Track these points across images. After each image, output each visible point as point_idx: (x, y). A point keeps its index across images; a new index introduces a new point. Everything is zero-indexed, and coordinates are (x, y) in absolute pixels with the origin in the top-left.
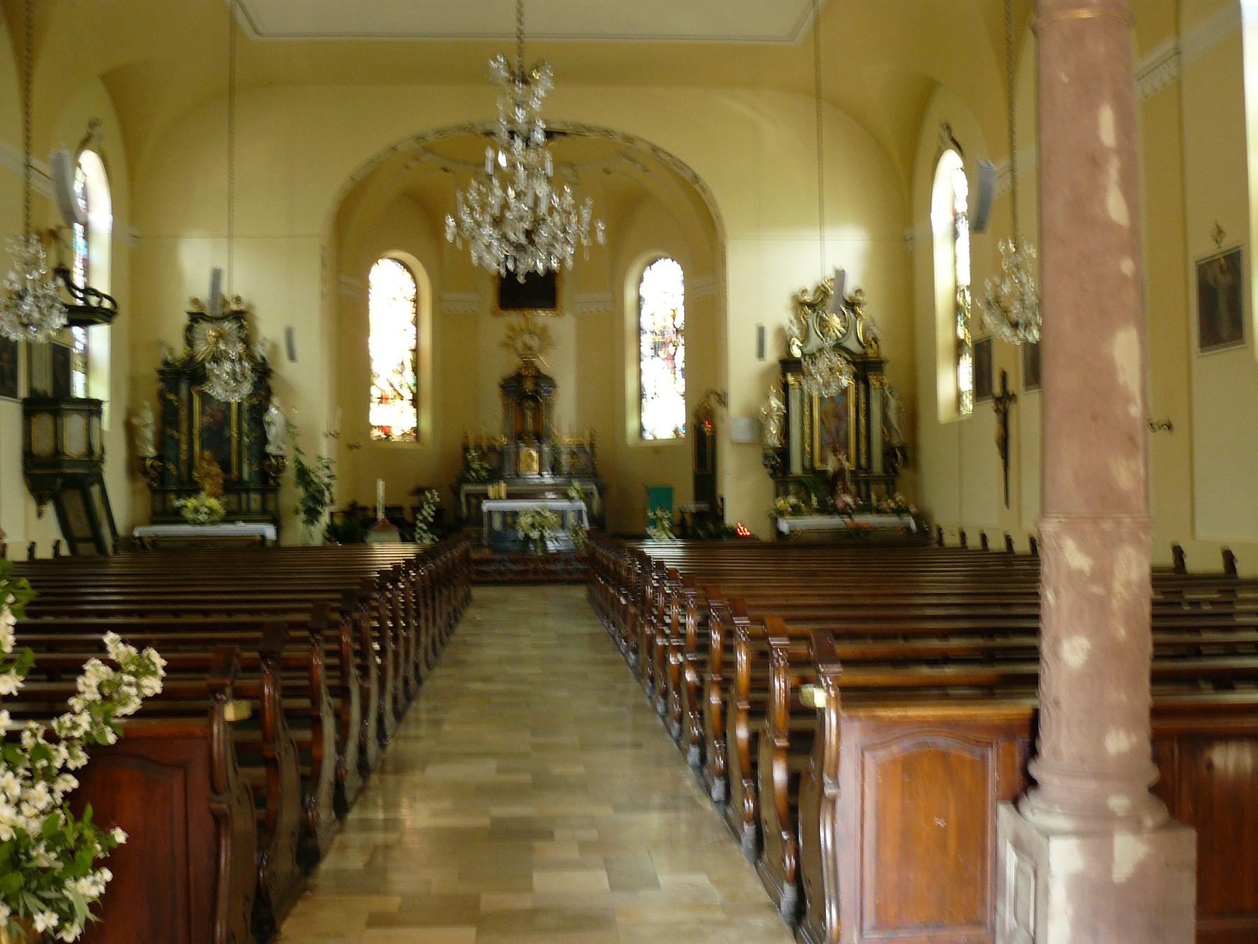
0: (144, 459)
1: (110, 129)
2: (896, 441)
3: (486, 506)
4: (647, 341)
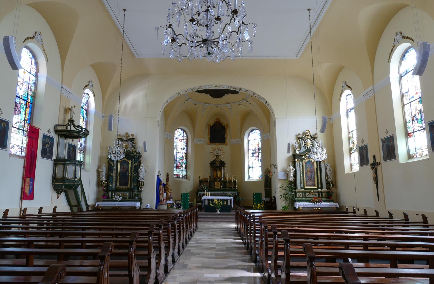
0: (102, 181)
1: (96, 83)
2: (329, 180)
3: (203, 198)
4: (250, 152)
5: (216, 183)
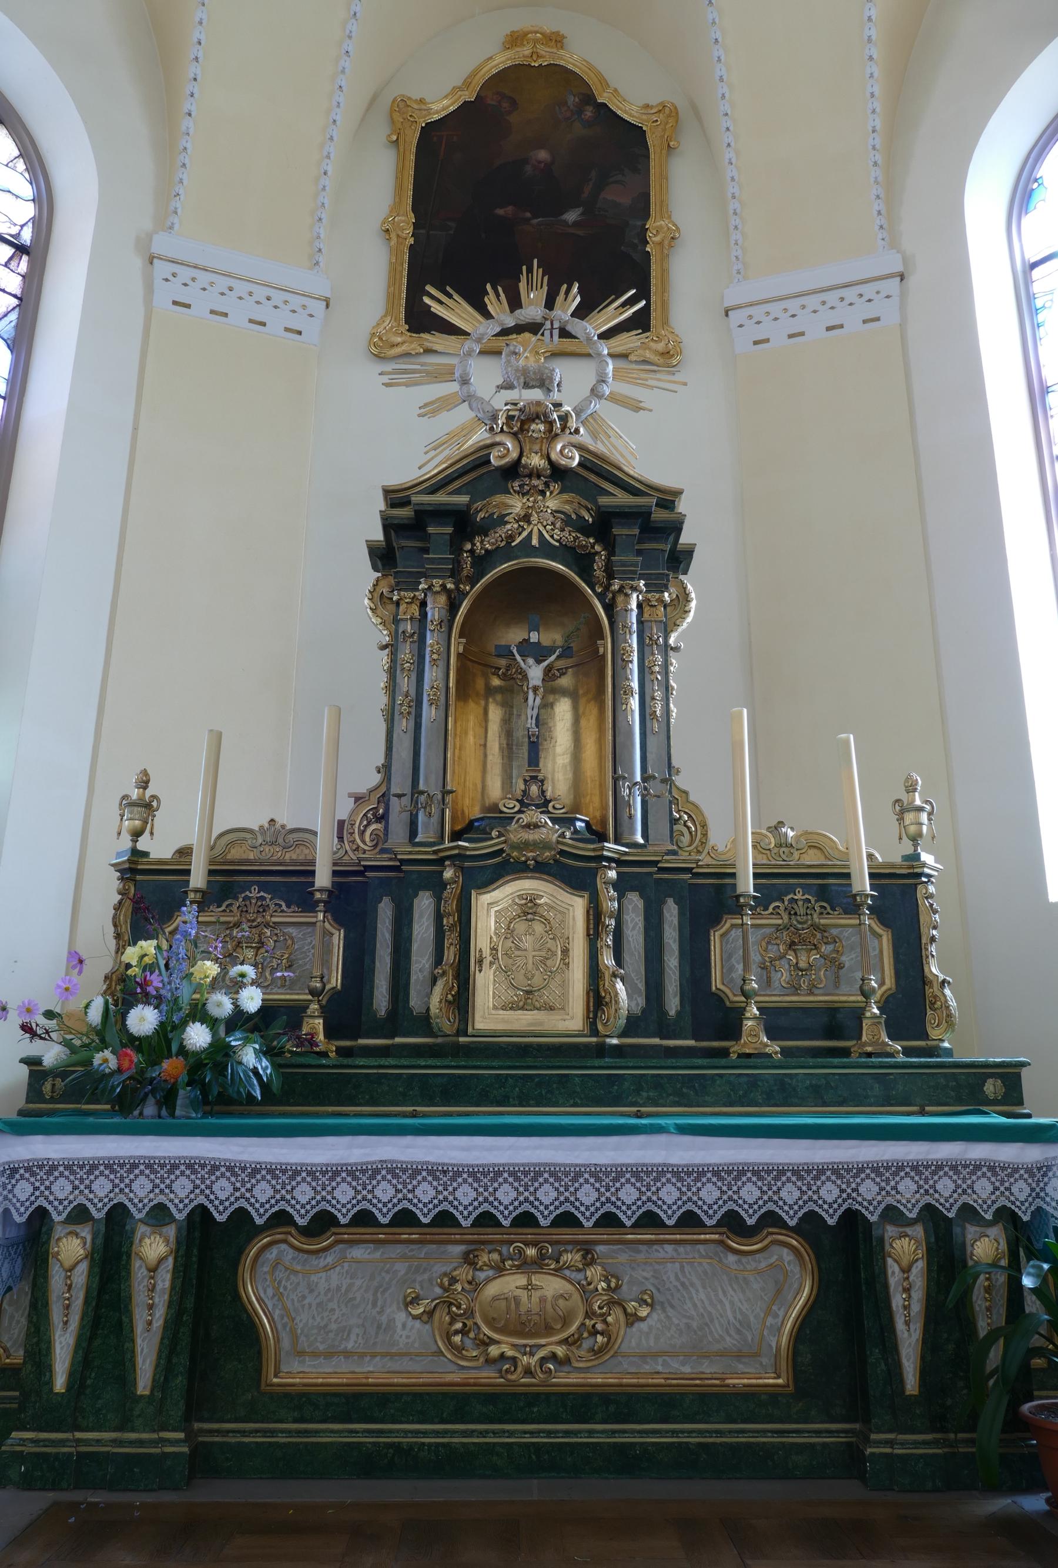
5: (492, 909)
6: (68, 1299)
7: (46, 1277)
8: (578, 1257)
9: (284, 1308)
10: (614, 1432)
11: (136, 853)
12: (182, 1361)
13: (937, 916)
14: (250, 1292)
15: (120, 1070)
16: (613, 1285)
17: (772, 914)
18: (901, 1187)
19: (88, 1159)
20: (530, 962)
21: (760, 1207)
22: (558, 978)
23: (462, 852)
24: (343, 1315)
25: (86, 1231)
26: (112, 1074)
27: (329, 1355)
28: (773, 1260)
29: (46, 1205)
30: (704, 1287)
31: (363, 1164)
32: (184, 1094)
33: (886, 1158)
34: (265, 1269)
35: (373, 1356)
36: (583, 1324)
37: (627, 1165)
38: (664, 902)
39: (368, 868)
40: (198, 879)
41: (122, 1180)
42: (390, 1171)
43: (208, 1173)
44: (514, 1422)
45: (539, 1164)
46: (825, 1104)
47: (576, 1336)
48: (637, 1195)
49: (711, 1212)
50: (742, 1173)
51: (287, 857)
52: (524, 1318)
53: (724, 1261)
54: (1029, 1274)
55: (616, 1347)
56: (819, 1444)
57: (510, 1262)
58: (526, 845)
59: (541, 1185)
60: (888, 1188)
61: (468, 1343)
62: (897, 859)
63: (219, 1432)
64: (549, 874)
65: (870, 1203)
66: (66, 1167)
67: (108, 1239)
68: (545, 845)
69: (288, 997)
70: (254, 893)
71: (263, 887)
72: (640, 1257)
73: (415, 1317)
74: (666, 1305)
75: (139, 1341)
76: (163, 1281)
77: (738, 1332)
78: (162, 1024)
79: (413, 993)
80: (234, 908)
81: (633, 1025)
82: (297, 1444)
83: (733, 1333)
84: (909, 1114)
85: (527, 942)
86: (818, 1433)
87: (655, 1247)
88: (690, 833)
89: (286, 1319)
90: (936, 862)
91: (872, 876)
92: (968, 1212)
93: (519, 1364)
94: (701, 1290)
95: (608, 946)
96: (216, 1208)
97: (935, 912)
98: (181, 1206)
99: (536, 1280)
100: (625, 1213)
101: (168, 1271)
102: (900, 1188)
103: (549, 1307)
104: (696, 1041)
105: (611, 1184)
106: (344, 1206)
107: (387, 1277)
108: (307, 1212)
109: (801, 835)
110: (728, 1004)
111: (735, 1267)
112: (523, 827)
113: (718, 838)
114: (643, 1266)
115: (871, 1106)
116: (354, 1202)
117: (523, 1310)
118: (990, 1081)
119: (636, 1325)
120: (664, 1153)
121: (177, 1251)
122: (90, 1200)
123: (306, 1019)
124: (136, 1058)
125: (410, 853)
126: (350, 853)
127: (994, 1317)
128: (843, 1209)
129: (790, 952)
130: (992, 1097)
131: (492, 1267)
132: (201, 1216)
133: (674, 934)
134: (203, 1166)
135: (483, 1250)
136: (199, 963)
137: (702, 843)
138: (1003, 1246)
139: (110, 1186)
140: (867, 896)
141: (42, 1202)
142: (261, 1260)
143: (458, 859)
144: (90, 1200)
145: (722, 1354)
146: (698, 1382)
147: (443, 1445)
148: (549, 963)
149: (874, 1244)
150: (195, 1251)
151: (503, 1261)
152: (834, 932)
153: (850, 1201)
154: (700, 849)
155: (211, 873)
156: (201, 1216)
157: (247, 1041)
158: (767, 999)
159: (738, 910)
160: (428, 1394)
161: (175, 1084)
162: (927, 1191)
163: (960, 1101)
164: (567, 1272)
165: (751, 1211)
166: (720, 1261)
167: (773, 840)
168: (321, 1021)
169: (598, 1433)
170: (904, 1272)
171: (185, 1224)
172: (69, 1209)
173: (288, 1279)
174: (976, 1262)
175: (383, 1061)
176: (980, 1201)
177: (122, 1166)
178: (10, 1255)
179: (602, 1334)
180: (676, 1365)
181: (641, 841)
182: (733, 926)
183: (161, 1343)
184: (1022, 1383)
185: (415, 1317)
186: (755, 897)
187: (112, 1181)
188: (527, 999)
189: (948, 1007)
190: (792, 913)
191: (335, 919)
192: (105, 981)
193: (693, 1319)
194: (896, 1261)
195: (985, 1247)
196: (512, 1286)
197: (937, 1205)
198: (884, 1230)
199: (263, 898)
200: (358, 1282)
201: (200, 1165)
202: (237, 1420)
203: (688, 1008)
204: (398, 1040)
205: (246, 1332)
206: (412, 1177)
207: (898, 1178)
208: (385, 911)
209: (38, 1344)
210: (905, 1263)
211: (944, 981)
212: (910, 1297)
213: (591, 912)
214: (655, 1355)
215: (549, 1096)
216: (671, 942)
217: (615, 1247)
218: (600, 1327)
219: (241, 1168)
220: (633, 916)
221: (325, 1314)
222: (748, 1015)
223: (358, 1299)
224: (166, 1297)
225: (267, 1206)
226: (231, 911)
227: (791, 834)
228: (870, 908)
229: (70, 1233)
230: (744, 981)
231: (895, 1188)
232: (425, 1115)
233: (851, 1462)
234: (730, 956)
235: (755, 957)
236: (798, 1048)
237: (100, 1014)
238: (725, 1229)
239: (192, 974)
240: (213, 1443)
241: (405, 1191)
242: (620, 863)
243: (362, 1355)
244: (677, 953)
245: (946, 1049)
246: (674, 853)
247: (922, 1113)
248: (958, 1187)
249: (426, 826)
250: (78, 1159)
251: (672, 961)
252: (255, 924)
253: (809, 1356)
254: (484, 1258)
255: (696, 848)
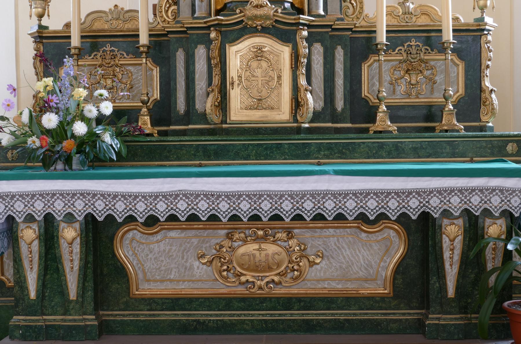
5: (237, 54)
6: (31, 257)
7: (18, 248)
8: (285, 235)
9: (138, 260)
10: (303, 314)
11: (40, 27)
12: (90, 284)
13: (491, 53)
14: (121, 253)
15: (42, 147)
16: (302, 248)
17: (397, 53)
18: (452, 201)
19: (31, 192)
20: (260, 83)
21: (377, 211)
22: (276, 92)
23: (220, 22)
24: (167, 263)
25: (35, 226)
26: (38, 149)
27: (162, 281)
28: (385, 236)
29: (12, 214)
30: (349, 249)
31: (170, 192)
32: (76, 159)
33: (445, 186)
34: (127, 242)
35: (184, 281)
36: (288, 266)
37: (307, 191)
38: (336, 48)
39: (169, 32)
40: (75, 41)
41: (49, 201)
42: (184, 195)
43: (91, 197)
44: (254, 310)
45: (261, 191)
46: (419, 157)
47: (284, 272)
48: (313, 205)
49: (351, 213)
50: (369, 194)
51: (126, 26)
52: (257, 264)
53: (360, 236)
54: (512, 243)
55: (304, 276)
56: (404, 319)
57: (250, 238)
58: (256, 18)
59: (263, 201)
60: (445, 201)
61: (230, 275)
62: (471, 21)
63: (112, 315)
64: (269, 34)
65: (435, 208)
66: (20, 196)
67: (46, 230)
68: (267, 17)
69: (132, 104)
70: (108, 48)
71: (112, 44)
72: (316, 235)
73: (203, 264)
74: (330, 257)
75: (68, 276)
76: (76, 248)
77: (366, 269)
78: (61, 122)
79: (197, 101)
80: (98, 57)
81: (317, 116)
82: (150, 320)
83: (363, 269)
84: (464, 162)
85: (258, 72)
86: (404, 314)
87: (325, 230)
88: (353, 7)
89: (139, 265)
90: (494, 22)
91: (454, 31)
92: (487, 213)
93: (256, 285)
94: (347, 250)
95: (303, 74)
96: (97, 214)
97: (490, 51)
98: (80, 214)
99: (263, 246)
100: (306, 214)
101: (78, 244)
102: (451, 201)
103: (270, 258)
104: (352, 124)
105: (299, 200)
106: (162, 212)
107: (188, 245)
108: (143, 216)
109: (417, 7)
110: (371, 104)
111: (365, 239)
112: (254, 7)
113: (369, 10)
114: (315, 239)
115: (444, 158)
116: (167, 210)
117: (257, 260)
118: (510, 144)
119: (314, 266)
120: (327, 184)
121: (81, 235)
122: (34, 211)
123: (140, 117)
124: (50, 140)
125: (191, 23)
126: (161, 23)
127: (496, 262)
128: (420, 211)
129: (407, 75)
130: (510, 152)
131: (241, 240)
132: (90, 219)
133: (341, 66)
134: (89, 194)
135: (236, 232)
136: (76, 89)
137: (360, 13)
138: (504, 228)
139: (43, 205)
140: (450, 43)
141: (10, 213)
142: (125, 238)
143: (218, 26)
144: (34, 211)
145: (357, 279)
146: (345, 292)
147: (220, 320)
148: (270, 83)
149: (437, 228)
150: (91, 235)
151: (246, 237)
152: (432, 63)
153: (425, 207)
154: (359, 16)
155: (82, 37)
156: (90, 219)
157: (105, 130)
158: (392, 101)
159: (377, 52)
160: (212, 298)
161: (70, 153)
162: (465, 202)
163: (492, 154)
164: (279, 242)
165: (372, 213)
166: (358, 236)
167: (401, 10)
168: (149, 117)
169: (296, 315)
170: (451, 241)
171: (84, 221)
172: (24, 216)
173: (139, 247)
174: (489, 236)
175: (182, 138)
176: (493, 207)
177: (48, 195)
178: (8, 235)
179: (297, 271)
180: (335, 285)
181: (322, 13)
182: (375, 61)
183: (79, 277)
184: (507, 291)
185: (203, 264)
186: (386, 45)
187: (44, 202)
188: (259, 103)
189: (493, 104)
190: (409, 53)
191: (154, 62)
192: (34, 98)
193: (343, 263)
194: (447, 236)
195: (495, 229)
196: (251, 249)
197: (470, 209)
198: (442, 221)
199: (113, 51)
200: (174, 248)
201: (87, 194)
202: (120, 310)
203: (348, 107)
204: (191, 126)
205: (120, 271)
206: (196, 198)
207: (450, 196)
208: (180, 56)
209: (19, 278)
210: (452, 237)
211: (492, 90)
212: (453, 253)
213: (293, 55)
214: (324, 280)
215: (271, 154)
216: (339, 70)
217: (304, 230)
218: (296, 267)
219: (108, 195)
220: (317, 56)
221: (159, 263)
222: (380, 110)
223: (175, 256)
224: (79, 256)
225: (123, 213)
226: (97, 58)
227: (412, 6)
228: (452, 50)
229: (27, 227)
230: (379, 91)
231: (449, 201)
232: (206, 166)
233: (419, 327)
234: (373, 78)
235: (386, 77)
236: (408, 127)
237: (28, 118)
238: (360, 221)
239: (73, 95)
240: (109, 320)
241: (192, 205)
242: (309, 26)
243: (178, 281)
244: (342, 76)
245: (490, 127)
246: (342, 20)
247: (472, 161)
248: (482, 200)
249: (200, 7)
250: (25, 192)
251: (340, 82)
252: (110, 65)
253: (401, 280)
254: (237, 236)
255: (356, 16)
